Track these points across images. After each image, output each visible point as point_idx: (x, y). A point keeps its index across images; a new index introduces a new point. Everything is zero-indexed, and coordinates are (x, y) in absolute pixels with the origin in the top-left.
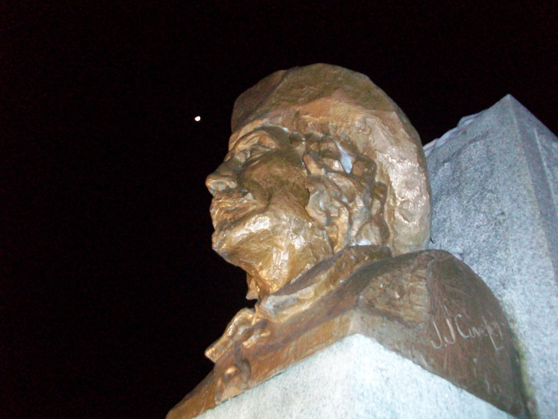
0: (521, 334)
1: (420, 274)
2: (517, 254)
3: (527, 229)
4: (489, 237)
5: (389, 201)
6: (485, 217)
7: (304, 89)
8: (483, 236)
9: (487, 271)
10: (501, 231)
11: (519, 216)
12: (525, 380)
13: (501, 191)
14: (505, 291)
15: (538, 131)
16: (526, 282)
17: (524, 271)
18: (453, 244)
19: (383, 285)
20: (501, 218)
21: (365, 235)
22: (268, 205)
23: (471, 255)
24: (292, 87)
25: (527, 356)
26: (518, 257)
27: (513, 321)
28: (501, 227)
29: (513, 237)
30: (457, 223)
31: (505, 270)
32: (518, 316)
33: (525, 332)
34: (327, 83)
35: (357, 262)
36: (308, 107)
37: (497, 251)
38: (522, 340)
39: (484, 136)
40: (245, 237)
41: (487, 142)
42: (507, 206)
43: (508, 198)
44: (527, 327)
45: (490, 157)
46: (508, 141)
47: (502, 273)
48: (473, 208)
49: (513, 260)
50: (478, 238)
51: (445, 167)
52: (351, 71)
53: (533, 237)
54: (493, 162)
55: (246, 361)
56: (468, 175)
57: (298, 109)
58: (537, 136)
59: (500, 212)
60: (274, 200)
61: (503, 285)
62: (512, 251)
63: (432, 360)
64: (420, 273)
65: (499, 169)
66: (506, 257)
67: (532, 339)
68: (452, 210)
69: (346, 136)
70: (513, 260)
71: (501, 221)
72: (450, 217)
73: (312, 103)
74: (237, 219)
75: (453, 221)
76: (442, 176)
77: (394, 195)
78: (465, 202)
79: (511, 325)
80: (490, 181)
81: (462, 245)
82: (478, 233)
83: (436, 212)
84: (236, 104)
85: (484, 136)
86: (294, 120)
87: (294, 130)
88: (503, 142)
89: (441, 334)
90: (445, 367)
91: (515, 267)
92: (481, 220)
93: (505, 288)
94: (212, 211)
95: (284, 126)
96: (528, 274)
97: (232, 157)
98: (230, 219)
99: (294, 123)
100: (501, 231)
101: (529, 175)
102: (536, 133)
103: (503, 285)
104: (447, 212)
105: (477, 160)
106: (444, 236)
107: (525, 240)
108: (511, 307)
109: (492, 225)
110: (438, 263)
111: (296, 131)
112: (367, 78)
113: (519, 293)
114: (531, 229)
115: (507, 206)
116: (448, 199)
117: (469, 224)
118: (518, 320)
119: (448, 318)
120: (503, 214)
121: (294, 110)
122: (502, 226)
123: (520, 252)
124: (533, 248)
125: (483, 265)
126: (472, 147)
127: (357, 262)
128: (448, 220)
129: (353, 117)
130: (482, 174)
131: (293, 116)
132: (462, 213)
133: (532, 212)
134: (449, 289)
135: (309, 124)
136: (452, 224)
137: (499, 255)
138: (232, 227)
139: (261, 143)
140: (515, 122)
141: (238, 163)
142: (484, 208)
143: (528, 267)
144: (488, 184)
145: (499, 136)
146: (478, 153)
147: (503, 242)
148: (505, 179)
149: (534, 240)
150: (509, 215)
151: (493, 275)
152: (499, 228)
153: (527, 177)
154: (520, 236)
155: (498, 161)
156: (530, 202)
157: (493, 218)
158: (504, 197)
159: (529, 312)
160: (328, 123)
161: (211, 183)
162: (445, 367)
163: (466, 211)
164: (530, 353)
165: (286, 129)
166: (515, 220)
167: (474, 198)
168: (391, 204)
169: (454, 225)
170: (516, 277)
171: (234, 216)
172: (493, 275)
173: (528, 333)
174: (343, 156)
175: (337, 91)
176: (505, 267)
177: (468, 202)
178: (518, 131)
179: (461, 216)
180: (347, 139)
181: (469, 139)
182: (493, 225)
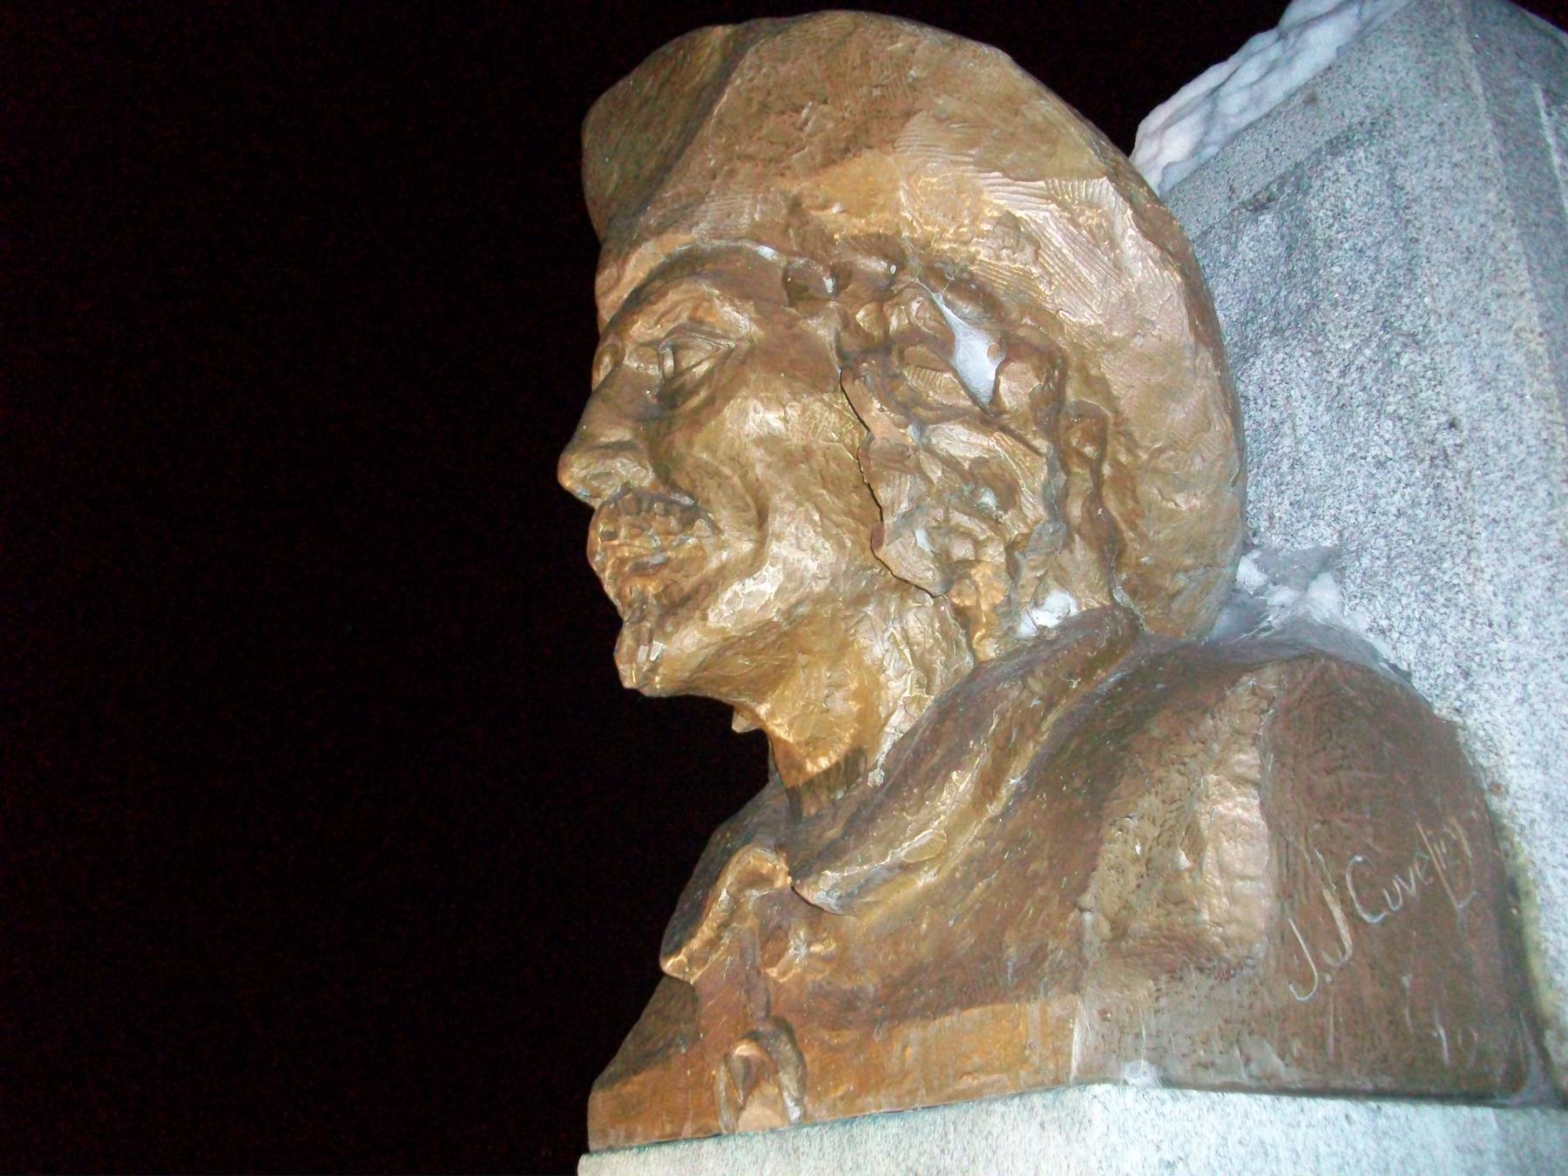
0: (1522, 827)
1: (1239, 770)
2: (1501, 570)
3: (1529, 489)
4: (1415, 503)
5: (1115, 452)
6: (1398, 432)
7: (805, 112)
8: (1397, 497)
9: (1415, 624)
10: (1452, 486)
11: (1502, 442)
12: (1536, 965)
13: (1442, 338)
14: (1473, 697)
15: (1547, 92)
16: (1532, 667)
17: (1524, 628)
18: (1307, 513)
19: (1143, 845)
20: (1448, 440)
21: (1056, 579)
22: (761, 543)
23: (1366, 561)
24: (765, 108)
25: (1539, 895)
26: (1505, 578)
27: (1496, 788)
28: (1449, 474)
29: (1486, 509)
30: (1312, 438)
31: (1468, 623)
32: (1511, 773)
33: (1533, 822)
34: (876, 92)
35: (1050, 704)
36: (825, 184)
37: (1441, 559)
38: (1524, 844)
39: (1375, 128)
40: (712, 650)
41: (1388, 152)
42: (1464, 396)
43: (1466, 368)
44: (1537, 807)
45: (1401, 212)
46: (1458, 157)
47: (1463, 633)
48: (1362, 396)
49: (1490, 588)
50: (1382, 502)
51: (1262, 229)
52: (949, 37)
53: (1551, 522)
54: (1412, 232)
55: (784, 1027)
56: (1336, 269)
57: (795, 190)
58: (1543, 115)
59: (1443, 418)
60: (775, 523)
61: (1466, 674)
62: (1486, 560)
63: (1296, 1046)
64: (1240, 763)
65: (1434, 257)
66: (1470, 579)
67: (1553, 849)
68: (1295, 393)
69: (963, 270)
70: (1490, 588)
71: (1450, 451)
72: (1290, 415)
73: (837, 170)
74: (677, 599)
75: (1301, 431)
76: (1252, 255)
77: (1128, 435)
78: (1335, 372)
79: (1494, 802)
80: (1406, 301)
81: (1336, 519)
82: (1380, 485)
83: (1246, 398)
84: (588, 138)
85: (1375, 128)
86: (788, 226)
87: (791, 253)
88: (1439, 156)
89: (1313, 948)
90: (1331, 1049)
91: (1498, 611)
92: (1387, 442)
93: (1471, 687)
94: (596, 562)
95: (760, 242)
96: (1536, 642)
97: (617, 363)
98: (657, 596)
99: (791, 232)
100: (1452, 486)
101: (1528, 296)
102: (1541, 102)
103: (1466, 674)
104: (1280, 402)
105: (1360, 216)
106: (1278, 485)
107: (1524, 525)
108: (1492, 748)
109: (1422, 460)
110: (1288, 710)
111: (800, 255)
112: (1004, 58)
113: (1512, 699)
114: (1541, 490)
115: (1464, 396)
116: (1281, 356)
117: (1350, 450)
118: (1512, 790)
119: (1328, 886)
120: (1453, 425)
121: (783, 193)
122: (1454, 470)
123: (1511, 563)
124: (1549, 558)
125: (1404, 601)
126: (1343, 170)
127: (1050, 704)
128: (1286, 428)
129: (975, 180)
130: (1378, 271)
131: (784, 211)
132: (1329, 409)
133: (1544, 435)
134: (1325, 783)
135: (836, 236)
136: (1298, 442)
137: (1450, 569)
138: (669, 629)
139: (701, 322)
140: (1478, 89)
141: (639, 381)
142: (1395, 402)
143: (1537, 619)
144: (1401, 310)
145: (1425, 130)
146: (1363, 187)
147: (1460, 526)
148: (1455, 298)
149: (1552, 532)
150: (1473, 429)
151: (1434, 639)
152: (1443, 476)
153: (1523, 303)
154: (1509, 510)
155: (1428, 229)
156: (1538, 398)
157: (1426, 441)
158: (1454, 362)
159: (1544, 764)
160: (899, 233)
161: (575, 474)
162: (1331, 1049)
163: (1341, 408)
164: (1548, 887)
165: (767, 252)
166: (1492, 451)
167: (1360, 360)
168: (1123, 458)
169: (1304, 447)
170: (1503, 645)
171: (667, 587)
172: (1434, 639)
173: (1543, 828)
174: (959, 336)
175: (914, 120)
176: (1468, 616)
177: (1343, 374)
178: (1489, 125)
179: (1326, 418)
180: (965, 275)
181: (1331, 127)
182: (1427, 463)
